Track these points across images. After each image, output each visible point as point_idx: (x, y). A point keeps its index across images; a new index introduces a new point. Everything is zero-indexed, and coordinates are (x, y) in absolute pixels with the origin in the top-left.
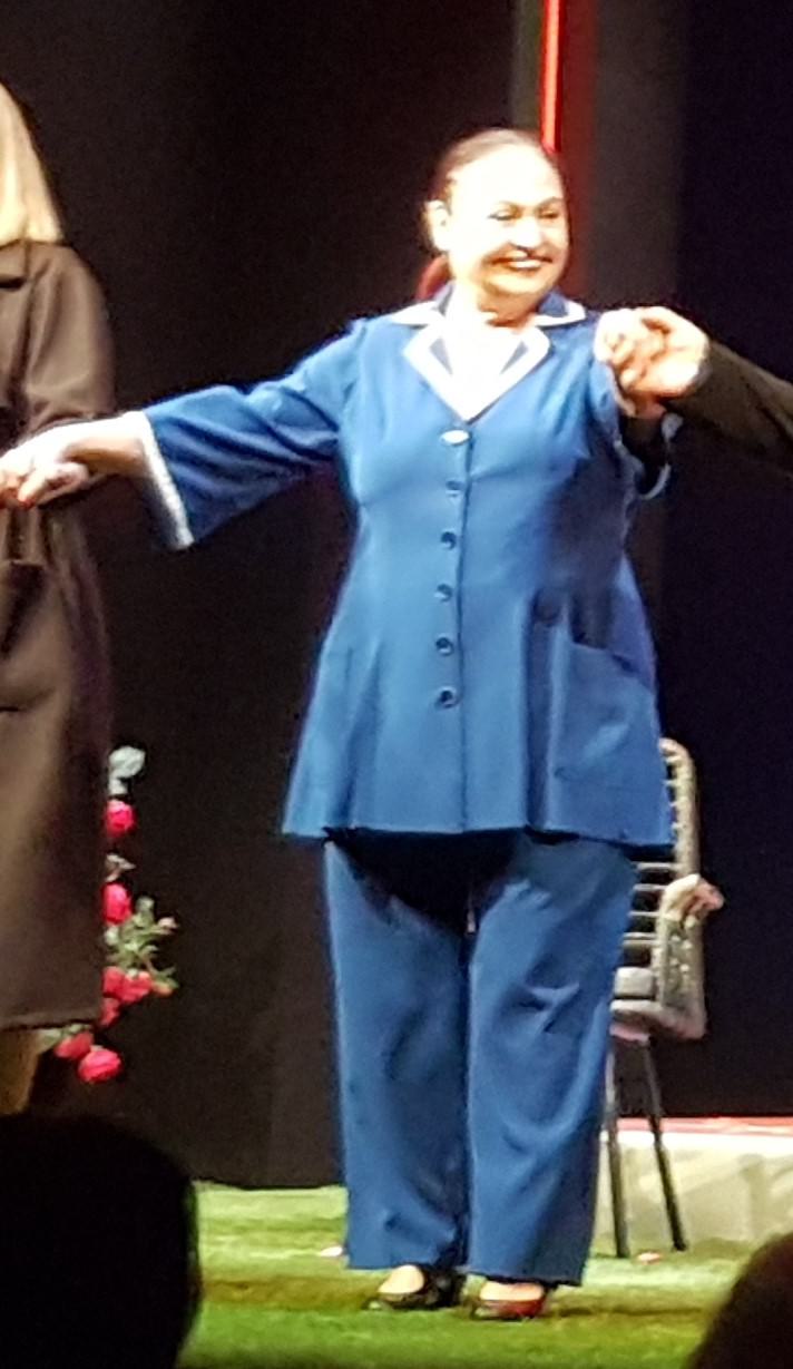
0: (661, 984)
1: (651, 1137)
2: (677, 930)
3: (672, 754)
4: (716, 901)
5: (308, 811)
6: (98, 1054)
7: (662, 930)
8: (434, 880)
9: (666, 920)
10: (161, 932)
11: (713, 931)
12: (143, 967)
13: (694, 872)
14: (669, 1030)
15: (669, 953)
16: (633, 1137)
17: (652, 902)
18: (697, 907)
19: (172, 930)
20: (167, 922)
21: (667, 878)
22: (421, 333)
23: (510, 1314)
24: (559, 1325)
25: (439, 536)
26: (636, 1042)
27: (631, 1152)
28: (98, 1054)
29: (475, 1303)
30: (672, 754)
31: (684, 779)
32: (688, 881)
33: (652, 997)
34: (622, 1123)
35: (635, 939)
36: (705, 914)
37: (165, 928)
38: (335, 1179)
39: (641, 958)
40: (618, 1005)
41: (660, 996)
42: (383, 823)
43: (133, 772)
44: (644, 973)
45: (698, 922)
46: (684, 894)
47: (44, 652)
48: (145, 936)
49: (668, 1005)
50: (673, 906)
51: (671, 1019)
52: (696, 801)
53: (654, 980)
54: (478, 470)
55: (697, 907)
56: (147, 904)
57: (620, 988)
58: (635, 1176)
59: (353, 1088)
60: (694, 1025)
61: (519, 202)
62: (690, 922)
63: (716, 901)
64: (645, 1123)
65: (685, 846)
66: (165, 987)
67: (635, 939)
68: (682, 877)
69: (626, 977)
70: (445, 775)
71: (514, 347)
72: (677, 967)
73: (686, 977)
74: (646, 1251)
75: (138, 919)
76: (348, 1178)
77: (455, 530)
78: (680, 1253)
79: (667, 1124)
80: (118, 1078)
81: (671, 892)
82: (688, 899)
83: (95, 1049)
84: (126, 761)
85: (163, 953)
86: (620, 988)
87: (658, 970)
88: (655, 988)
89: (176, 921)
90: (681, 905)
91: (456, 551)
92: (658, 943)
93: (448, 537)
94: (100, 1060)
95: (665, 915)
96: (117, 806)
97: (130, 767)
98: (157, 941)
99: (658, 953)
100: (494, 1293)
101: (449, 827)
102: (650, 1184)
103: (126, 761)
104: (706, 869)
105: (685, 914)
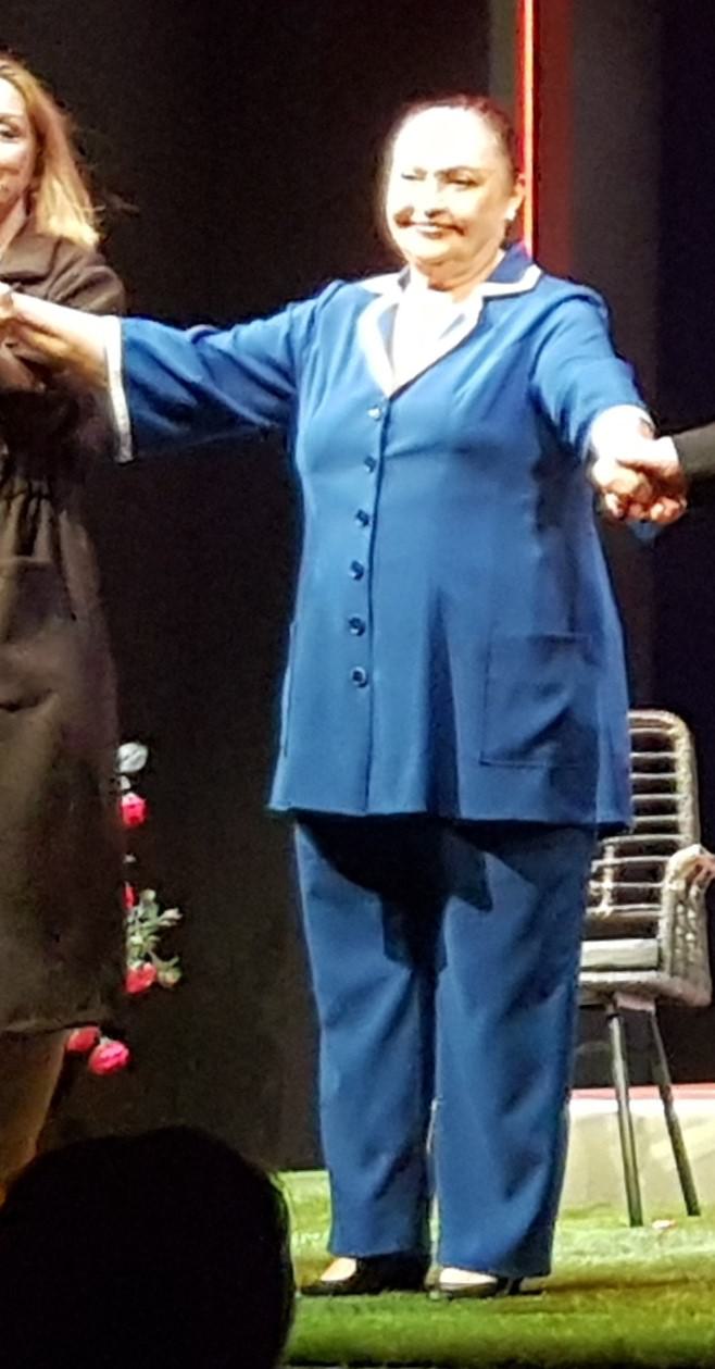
0: (667, 954)
1: (660, 1104)
2: (681, 900)
3: (669, 726)
5: (278, 801)
6: (108, 1046)
7: (666, 899)
8: (404, 866)
9: (671, 890)
10: (166, 923)
12: (147, 958)
13: (696, 842)
14: (677, 999)
15: (674, 924)
17: (655, 873)
18: (701, 876)
19: (178, 921)
20: (172, 914)
21: (671, 848)
22: (399, 312)
25: (355, 512)
26: (643, 1012)
27: (641, 1120)
28: (108, 1046)
29: (436, 1286)
30: (669, 726)
31: (682, 752)
32: (690, 852)
33: (658, 968)
34: (633, 1091)
36: (707, 883)
37: (171, 920)
38: (316, 1164)
40: (584, 977)
41: (667, 965)
42: (341, 804)
43: (139, 766)
44: (651, 943)
45: (703, 892)
46: (687, 864)
47: (49, 655)
48: (148, 928)
49: (673, 974)
50: (677, 875)
51: (678, 987)
52: (695, 771)
53: (660, 950)
54: (390, 450)
55: (701, 876)
56: (151, 895)
57: (584, 962)
58: (647, 1143)
59: (652, 1046)
60: (699, 992)
61: (424, 166)
62: (694, 891)
64: (655, 1091)
65: (686, 816)
66: (170, 976)
68: (685, 846)
70: (346, 759)
71: (456, 316)
72: (683, 936)
73: (691, 946)
74: (660, 1218)
75: (140, 910)
76: (328, 1162)
77: (369, 509)
78: (693, 1219)
79: (676, 1091)
80: (131, 1065)
81: (674, 862)
82: (692, 868)
83: (104, 1041)
84: (131, 756)
85: (166, 944)
86: (584, 962)
88: (661, 959)
89: (181, 912)
90: (685, 874)
91: (367, 532)
92: (663, 913)
93: (362, 517)
94: (110, 1051)
95: (669, 886)
96: (130, 799)
97: (134, 763)
98: (160, 932)
99: (663, 925)
100: (453, 1277)
101: (349, 810)
102: (662, 1150)
103: (131, 756)
104: (710, 837)
105: (689, 885)
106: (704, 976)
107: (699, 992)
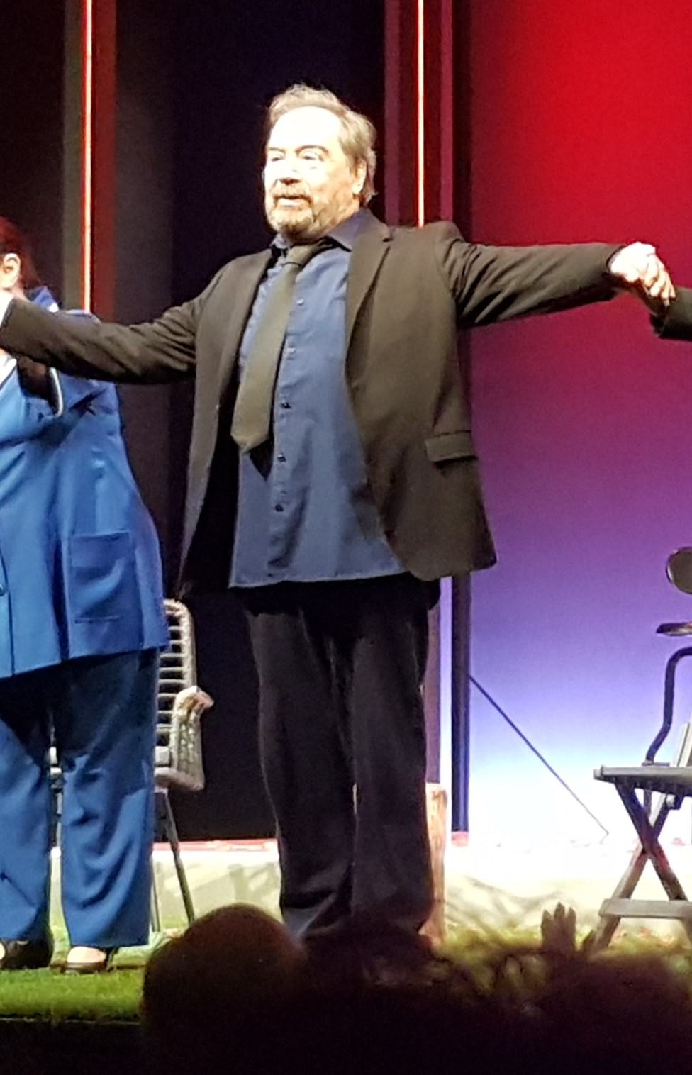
2: (184, 721)
4: (208, 702)
11: (207, 722)
16: (161, 855)
17: (168, 704)
21: (177, 689)
23: (86, 970)
24: (116, 976)
31: (185, 626)
35: (160, 728)
39: (164, 741)
51: (183, 778)
60: (198, 783)
63: (208, 702)
65: (187, 668)
67: (160, 728)
69: (160, 753)
81: (180, 697)
87: (176, 752)
92: (173, 730)
95: (177, 713)
104: (201, 683)
106: (199, 771)
107: (198, 783)
